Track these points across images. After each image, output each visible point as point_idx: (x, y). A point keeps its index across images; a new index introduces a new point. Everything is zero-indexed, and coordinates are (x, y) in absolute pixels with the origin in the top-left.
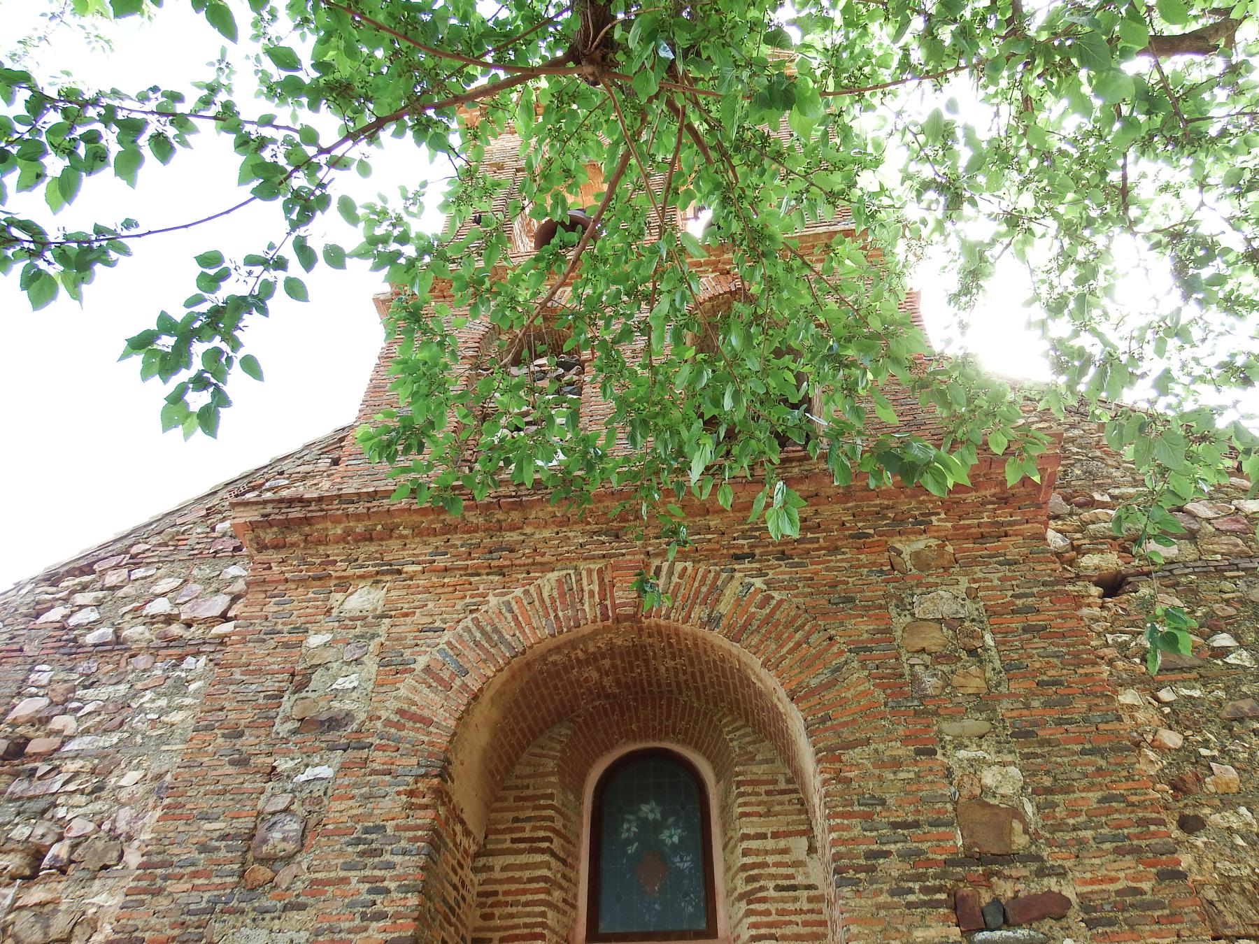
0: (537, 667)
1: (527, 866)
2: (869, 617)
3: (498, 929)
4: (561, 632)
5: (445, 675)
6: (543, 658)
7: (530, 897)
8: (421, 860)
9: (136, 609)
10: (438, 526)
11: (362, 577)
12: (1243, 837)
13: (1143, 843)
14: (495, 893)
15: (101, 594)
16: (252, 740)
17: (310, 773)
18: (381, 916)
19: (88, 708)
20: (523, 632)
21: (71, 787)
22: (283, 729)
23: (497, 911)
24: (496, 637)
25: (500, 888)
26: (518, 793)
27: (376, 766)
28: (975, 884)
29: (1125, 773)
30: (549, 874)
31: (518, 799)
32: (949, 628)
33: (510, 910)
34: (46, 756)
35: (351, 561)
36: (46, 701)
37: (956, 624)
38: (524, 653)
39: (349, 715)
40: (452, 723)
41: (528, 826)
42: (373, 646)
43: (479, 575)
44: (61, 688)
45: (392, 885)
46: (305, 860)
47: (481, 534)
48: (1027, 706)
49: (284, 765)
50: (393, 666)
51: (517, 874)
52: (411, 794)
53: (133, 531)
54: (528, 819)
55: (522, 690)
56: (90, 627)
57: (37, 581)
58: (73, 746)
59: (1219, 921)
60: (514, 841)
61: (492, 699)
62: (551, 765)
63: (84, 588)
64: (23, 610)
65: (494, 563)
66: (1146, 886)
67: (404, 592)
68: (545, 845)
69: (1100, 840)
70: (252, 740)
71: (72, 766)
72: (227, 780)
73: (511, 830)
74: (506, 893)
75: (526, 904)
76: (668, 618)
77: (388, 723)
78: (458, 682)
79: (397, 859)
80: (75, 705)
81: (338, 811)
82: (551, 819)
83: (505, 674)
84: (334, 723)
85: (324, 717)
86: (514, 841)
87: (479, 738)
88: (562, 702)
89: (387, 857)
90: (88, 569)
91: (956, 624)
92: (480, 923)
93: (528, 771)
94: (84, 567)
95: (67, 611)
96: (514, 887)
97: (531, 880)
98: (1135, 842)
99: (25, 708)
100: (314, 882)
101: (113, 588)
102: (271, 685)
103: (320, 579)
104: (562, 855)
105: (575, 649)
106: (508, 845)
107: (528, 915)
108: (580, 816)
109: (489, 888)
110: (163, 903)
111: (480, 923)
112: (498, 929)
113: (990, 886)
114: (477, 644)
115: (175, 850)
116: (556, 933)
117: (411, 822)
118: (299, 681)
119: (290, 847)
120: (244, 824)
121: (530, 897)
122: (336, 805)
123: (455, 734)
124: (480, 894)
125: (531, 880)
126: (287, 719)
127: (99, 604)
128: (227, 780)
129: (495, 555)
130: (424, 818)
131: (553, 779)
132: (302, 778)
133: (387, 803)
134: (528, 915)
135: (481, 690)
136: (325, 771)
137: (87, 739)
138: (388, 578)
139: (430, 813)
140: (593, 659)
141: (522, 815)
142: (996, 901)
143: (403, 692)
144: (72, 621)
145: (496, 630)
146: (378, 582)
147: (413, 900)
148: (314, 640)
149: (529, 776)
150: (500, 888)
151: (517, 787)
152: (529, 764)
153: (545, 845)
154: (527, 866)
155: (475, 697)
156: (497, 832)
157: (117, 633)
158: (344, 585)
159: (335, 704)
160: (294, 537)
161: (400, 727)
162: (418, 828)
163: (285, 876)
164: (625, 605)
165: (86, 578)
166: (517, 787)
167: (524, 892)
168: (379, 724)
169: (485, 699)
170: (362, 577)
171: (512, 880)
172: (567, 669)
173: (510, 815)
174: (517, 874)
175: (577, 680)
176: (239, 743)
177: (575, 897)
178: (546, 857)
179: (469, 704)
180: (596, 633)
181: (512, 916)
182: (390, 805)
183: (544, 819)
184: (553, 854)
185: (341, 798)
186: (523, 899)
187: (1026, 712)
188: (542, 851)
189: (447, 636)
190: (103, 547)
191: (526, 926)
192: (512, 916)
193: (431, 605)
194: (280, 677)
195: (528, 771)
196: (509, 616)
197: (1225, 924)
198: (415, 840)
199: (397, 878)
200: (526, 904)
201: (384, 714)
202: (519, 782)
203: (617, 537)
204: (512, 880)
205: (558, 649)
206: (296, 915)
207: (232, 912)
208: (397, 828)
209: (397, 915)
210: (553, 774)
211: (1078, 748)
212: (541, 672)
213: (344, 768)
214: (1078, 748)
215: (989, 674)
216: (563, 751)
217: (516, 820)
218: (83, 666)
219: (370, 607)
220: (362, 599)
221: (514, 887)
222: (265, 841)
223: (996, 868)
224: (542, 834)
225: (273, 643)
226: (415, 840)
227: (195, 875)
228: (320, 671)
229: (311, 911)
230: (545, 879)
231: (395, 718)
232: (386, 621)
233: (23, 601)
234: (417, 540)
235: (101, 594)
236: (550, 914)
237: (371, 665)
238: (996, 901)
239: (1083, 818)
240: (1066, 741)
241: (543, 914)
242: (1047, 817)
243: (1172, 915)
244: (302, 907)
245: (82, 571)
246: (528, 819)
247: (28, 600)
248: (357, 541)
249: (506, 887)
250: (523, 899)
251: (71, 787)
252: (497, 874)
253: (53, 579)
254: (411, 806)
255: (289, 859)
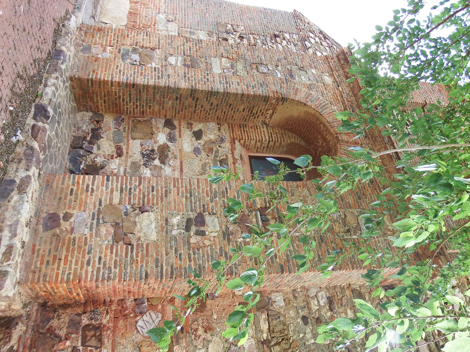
0: (318, 122)
1: (265, 136)
2: (354, 203)
3: (249, 129)
4: (329, 123)
5: (310, 97)
6: (321, 123)
7: (257, 136)
8: (261, 94)
9: (317, 50)
10: (356, 92)
11: (335, 79)
12: (303, 337)
13: (291, 263)
14: (257, 129)
15: (319, 42)
16: (284, 62)
17: (279, 73)
18: (248, 88)
19: (289, 46)
20: (327, 114)
21: (270, 47)
22: (288, 67)
23: (253, 129)
24: (324, 108)
25: (259, 130)
26: (284, 133)
27: (282, 85)
28: (272, 214)
29: (314, 265)
30: (264, 141)
31: (282, 133)
32: (356, 226)
33: (254, 132)
34: (276, 42)
35: (339, 76)
36: (289, 38)
37: (358, 228)
38: (321, 115)
39: (295, 79)
40: (297, 99)
41: (275, 135)
42: (315, 83)
43: (343, 104)
44: (293, 40)
45: (255, 89)
46: (258, 74)
47: (356, 103)
48: (332, 242)
49: (279, 68)
50: (310, 87)
51: (263, 133)
52: (277, 92)
53: (339, 45)
54: (277, 136)
55: (311, 121)
56: (310, 42)
57: (319, 29)
58: (279, 45)
59: (274, 318)
60: (271, 133)
61: (306, 111)
62: (293, 140)
63: (320, 39)
64: (311, 29)
65: (347, 107)
66: (278, 260)
67: (332, 87)
68: (271, 139)
69: (290, 251)
70: (284, 62)
71: (274, 46)
72: (274, 58)
73: (273, 132)
74: (258, 131)
75: (256, 136)
76: (340, 149)
77: (294, 87)
78: (308, 100)
79: (261, 90)
80: (289, 43)
81: (270, 79)
82: (278, 141)
83: (313, 112)
84: (291, 76)
85: (293, 74)
86: (271, 133)
87: (295, 112)
88: (311, 138)
89: (261, 88)
90: (325, 38)
91: (358, 228)
92: (250, 126)
93: (290, 135)
94: (326, 37)
95: (313, 37)
96: (259, 133)
97: (261, 136)
98: (291, 261)
99: (287, 36)
100: (254, 76)
101: (322, 44)
102: (299, 63)
103: (332, 70)
104: (269, 146)
105: (326, 131)
106: (270, 131)
107: (253, 136)
108: (281, 154)
109: (258, 127)
110: (246, 51)
111: (250, 126)
112: (249, 129)
113: (272, 218)
114: (321, 104)
115: (257, 52)
116: (250, 143)
117: (270, 92)
118: (301, 69)
119: (261, 71)
120: (265, 63)
121: (257, 136)
122: (271, 78)
123: (294, 100)
124: (257, 126)
125: (261, 136)
126: (291, 68)
127: (316, 43)
128: (274, 58)
129: (350, 107)
130: (271, 95)
131: (289, 142)
132: (277, 72)
133: (274, 87)
134: (253, 136)
135: (307, 105)
136: (279, 76)
137: (281, 47)
138: (336, 84)
139: (273, 96)
140: (324, 139)
141: (278, 134)
142: (269, 220)
143: (303, 89)
144: (310, 39)
145: (326, 109)
146: (334, 82)
147: (252, 93)
148: (313, 71)
149: (289, 136)
150: (259, 130)
151: (285, 133)
152: (292, 136)
153: (271, 139)
154: (265, 136)
155: (305, 104)
156: (273, 129)
157: (310, 47)
158: (332, 75)
159: (297, 76)
160: (342, 62)
161: (293, 89)
162: (269, 93)
163: (255, 71)
164: (342, 137)
165: (323, 38)
166: (285, 133)
167: (258, 135)
168: (293, 85)
169: (306, 109)
170: (335, 79)
171: (261, 132)
172: (320, 134)
173: (277, 132)
174: (263, 133)
175: (318, 139)
176: (283, 59)
177: (259, 152)
178: (268, 140)
179: (303, 103)
180: (331, 134)
181: (252, 132)
182: (273, 88)
183: (278, 139)
184: (269, 142)
185: (273, 79)
186: (257, 135)
187: (330, 241)
188: (269, 139)
189: (321, 98)
190: (333, 40)
191: (250, 136)
192: (252, 132)
193: (330, 94)
194: (302, 65)
195: (290, 135)
196: (331, 111)
197: (272, 320)
198: (266, 93)
199: (256, 90)
200: (256, 136)
201: (296, 86)
202: (287, 134)
203: (366, 137)
204: (261, 132)
205: (325, 126)
206: (246, 73)
207: (245, 63)
208: (268, 90)
209: (248, 91)
210: (290, 141)
211: (320, 254)
212: (317, 125)
213: (281, 79)
214: (320, 254)
215: (341, 234)
216: (297, 144)
217: (276, 133)
218: (299, 43)
219: (326, 81)
220: (328, 80)
221: (259, 133)
222: (261, 66)
223: (278, 220)
224: (274, 139)
225: (310, 63)
226: (266, 93)
227: (252, 56)
228: (305, 73)
229: (247, 76)
230: (262, 140)
231: (296, 88)
232: (323, 85)
233: (314, 28)
234: (350, 89)
235: (319, 42)
236: (254, 141)
237: (309, 82)
238: (269, 220)
239: (297, 249)
240: (321, 251)
241: (254, 139)
242: (295, 238)
243: (270, 265)
244: (248, 74)
245: (325, 38)
246: (277, 136)
247: (314, 29)
248: (345, 76)
249: (259, 131)
250: (257, 135)
251: (270, 47)
252: (262, 129)
253: (321, 32)
254: (274, 92)
255: (258, 71)
